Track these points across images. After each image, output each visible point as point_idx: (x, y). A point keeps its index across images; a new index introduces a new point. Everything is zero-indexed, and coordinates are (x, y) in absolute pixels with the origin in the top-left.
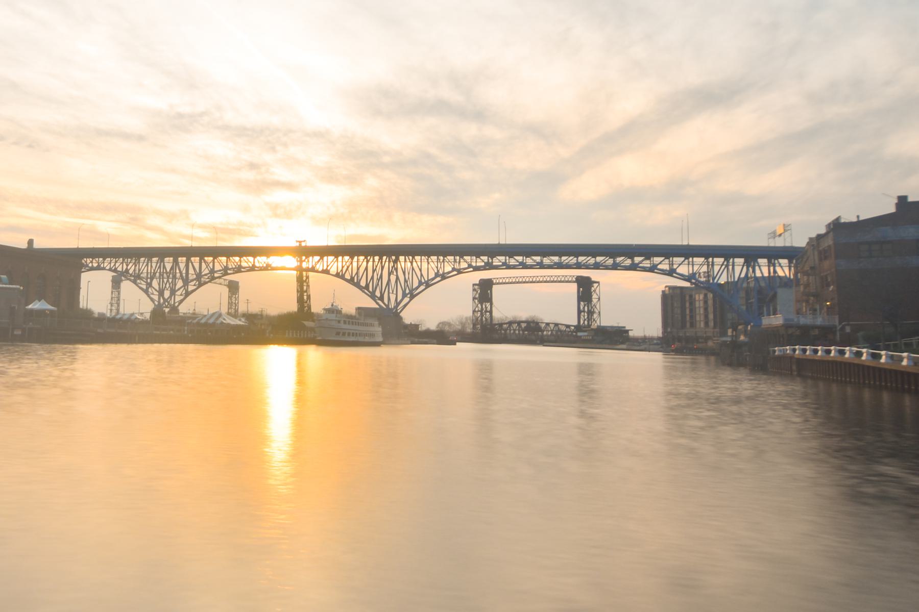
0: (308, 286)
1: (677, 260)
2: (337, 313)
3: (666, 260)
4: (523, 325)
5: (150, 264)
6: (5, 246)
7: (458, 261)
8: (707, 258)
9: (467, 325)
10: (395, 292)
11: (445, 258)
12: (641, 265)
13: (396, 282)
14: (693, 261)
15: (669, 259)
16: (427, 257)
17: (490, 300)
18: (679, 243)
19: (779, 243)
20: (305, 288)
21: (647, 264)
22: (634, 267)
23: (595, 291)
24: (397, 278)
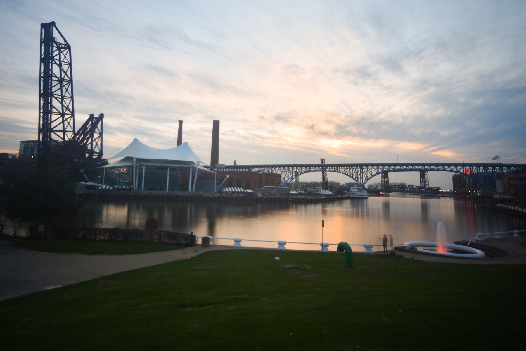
0: (326, 174)
4: (400, 186)
5: (368, 169)
8: (463, 167)
9: (378, 185)
14: (465, 168)
17: (388, 177)
20: (325, 175)
21: (449, 169)
22: (445, 170)
23: (426, 174)
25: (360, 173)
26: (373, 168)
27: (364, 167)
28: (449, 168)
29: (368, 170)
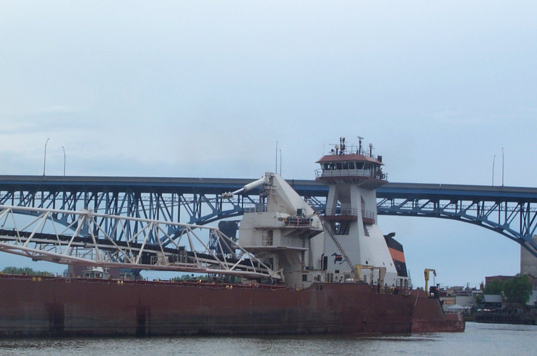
1: (489, 204)
2: (166, 235)
6: (146, 192)
11: (181, 197)
12: (445, 210)
14: (43, 195)
15: (456, 203)
16: (157, 195)
21: (451, 209)
22: (437, 213)
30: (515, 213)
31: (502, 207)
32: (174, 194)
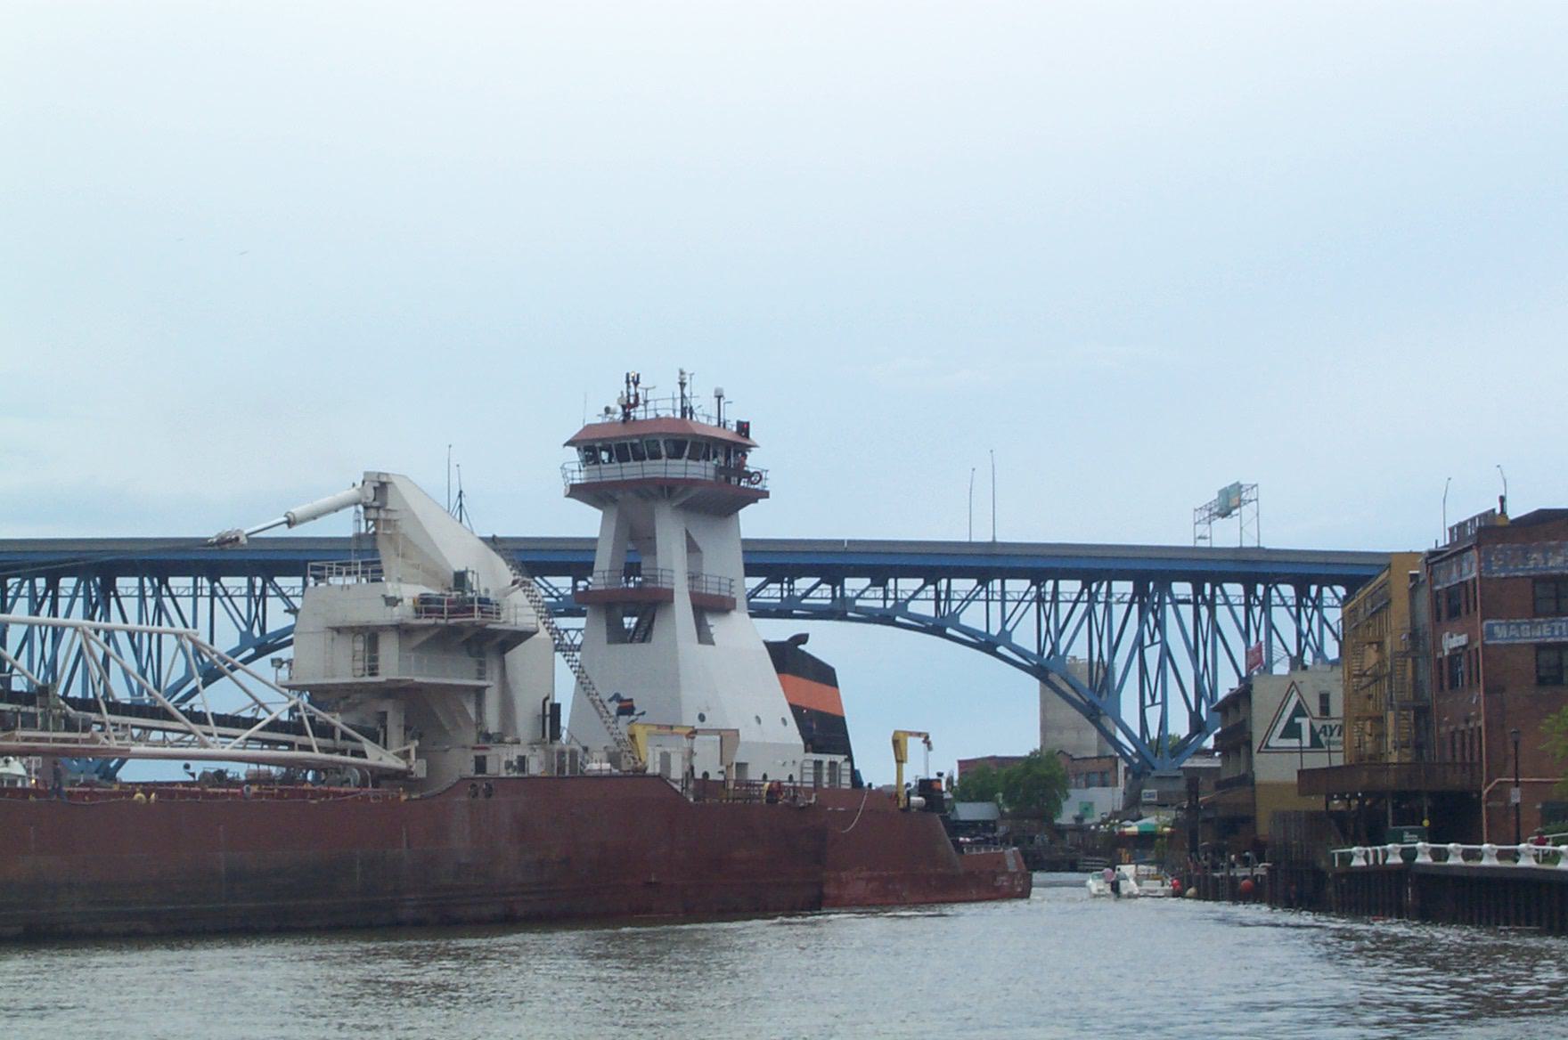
1: (963, 586)
3: (822, 586)
5: (167, 602)
7: (258, 592)
8: (984, 580)
10: (1158, 699)
12: (859, 603)
13: (1161, 666)
14: (1003, 592)
16: (156, 580)
18: (960, 536)
19: (1226, 535)
21: (873, 599)
24: (1166, 653)
25: (1139, 644)
26: (213, 594)
27: (127, 584)
28: (880, 592)
29: (160, 608)
30: (1023, 605)
31: (993, 592)
32: (199, 579)
